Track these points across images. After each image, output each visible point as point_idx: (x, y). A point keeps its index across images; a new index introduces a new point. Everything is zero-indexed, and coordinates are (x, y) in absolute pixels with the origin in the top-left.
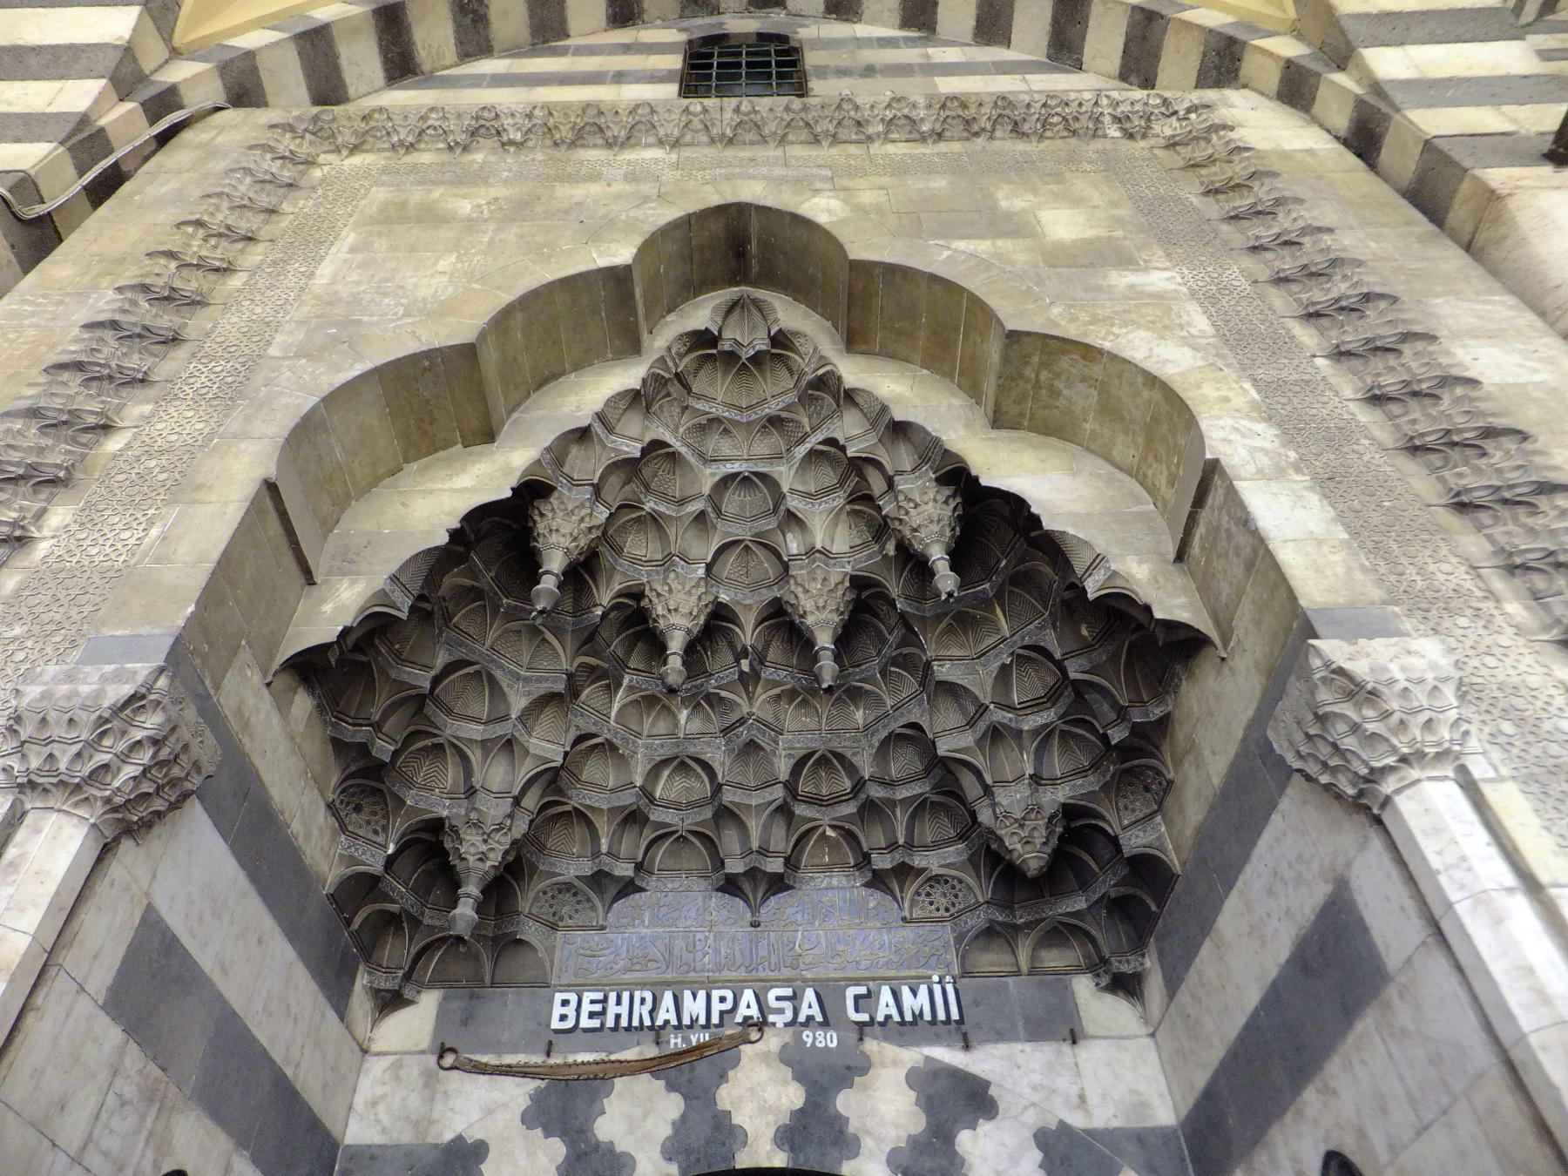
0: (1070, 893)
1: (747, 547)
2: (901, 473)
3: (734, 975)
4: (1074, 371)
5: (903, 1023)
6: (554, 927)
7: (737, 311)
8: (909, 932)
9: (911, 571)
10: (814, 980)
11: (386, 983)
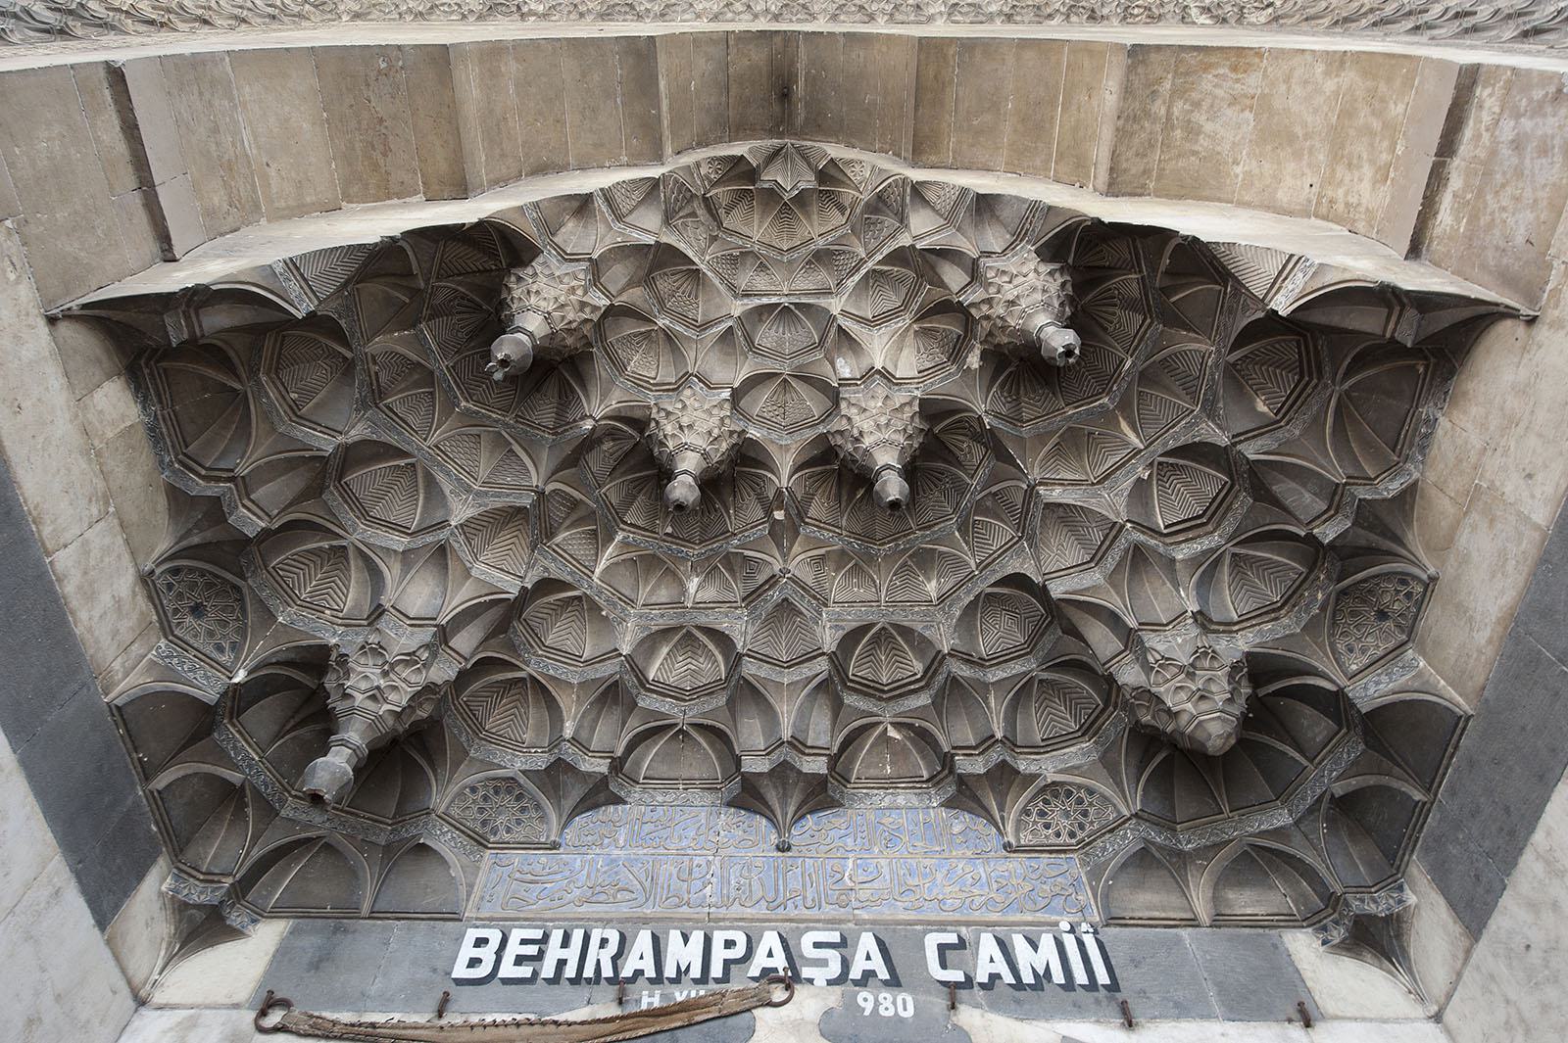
0: (1264, 804)
1: (785, 380)
2: (989, 254)
3: (749, 912)
4: (1220, 92)
5: (1019, 985)
6: (481, 843)
7: (779, 160)
8: (1017, 864)
9: (1002, 386)
10: (874, 922)
11: (199, 894)
